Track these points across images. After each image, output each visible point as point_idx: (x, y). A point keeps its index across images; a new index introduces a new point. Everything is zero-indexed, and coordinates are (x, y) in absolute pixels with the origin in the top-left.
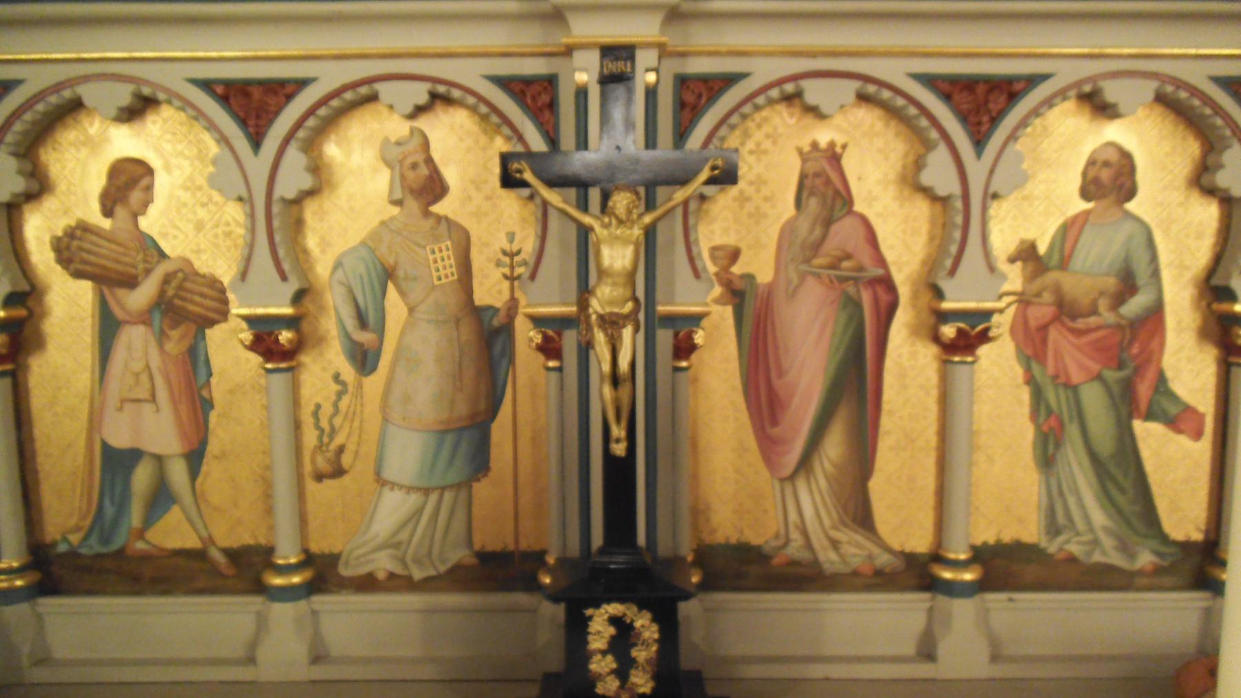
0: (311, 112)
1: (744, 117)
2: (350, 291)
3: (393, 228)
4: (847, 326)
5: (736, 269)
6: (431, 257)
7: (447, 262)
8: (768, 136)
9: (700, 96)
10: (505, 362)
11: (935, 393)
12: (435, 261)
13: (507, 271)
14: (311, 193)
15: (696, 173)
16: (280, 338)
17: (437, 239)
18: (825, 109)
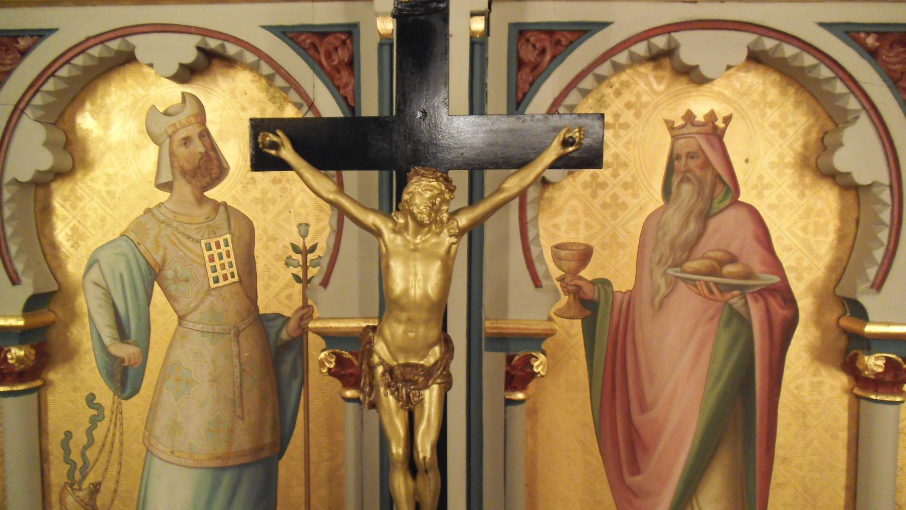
0: (48, 72)
1: (600, 79)
2: (108, 293)
3: (162, 218)
4: (731, 348)
5: (587, 274)
6: (207, 254)
7: (226, 260)
8: (629, 105)
9: (543, 52)
10: (296, 384)
11: (844, 435)
12: (212, 259)
13: (299, 271)
14: (59, 174)
15: (539, 151)
16: (9, 356)
17: (214, 233)
18: (705, 71)
